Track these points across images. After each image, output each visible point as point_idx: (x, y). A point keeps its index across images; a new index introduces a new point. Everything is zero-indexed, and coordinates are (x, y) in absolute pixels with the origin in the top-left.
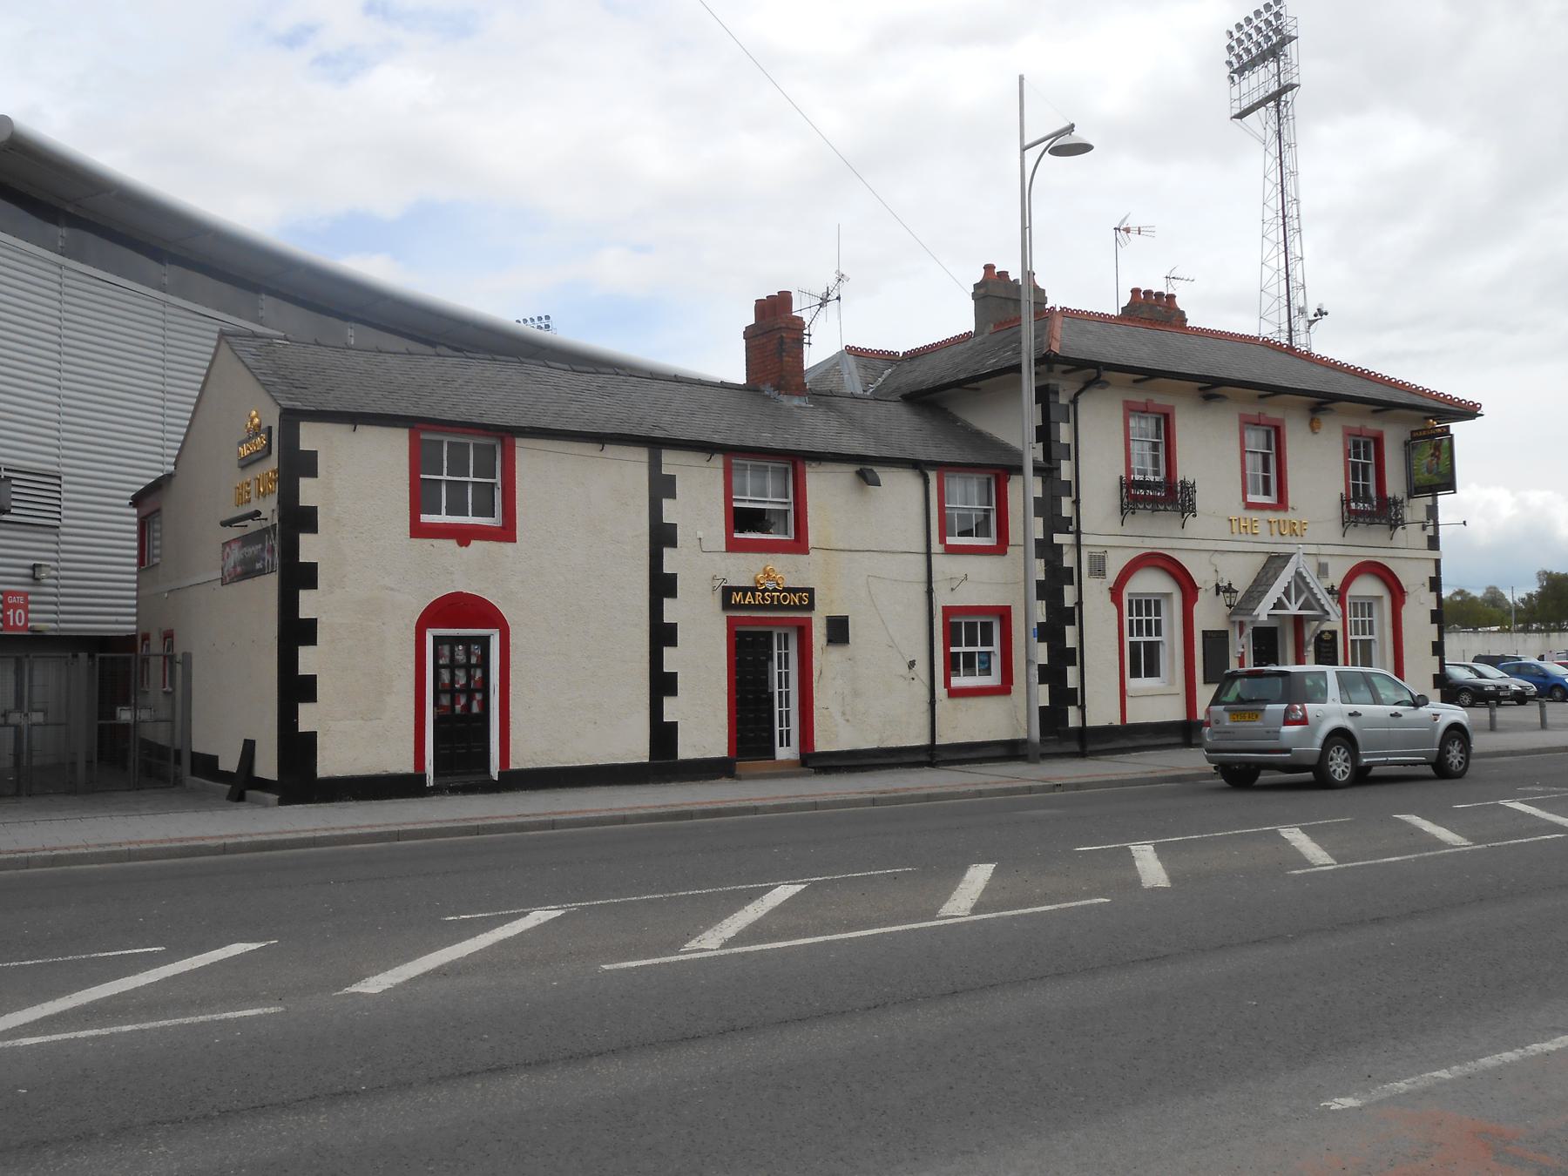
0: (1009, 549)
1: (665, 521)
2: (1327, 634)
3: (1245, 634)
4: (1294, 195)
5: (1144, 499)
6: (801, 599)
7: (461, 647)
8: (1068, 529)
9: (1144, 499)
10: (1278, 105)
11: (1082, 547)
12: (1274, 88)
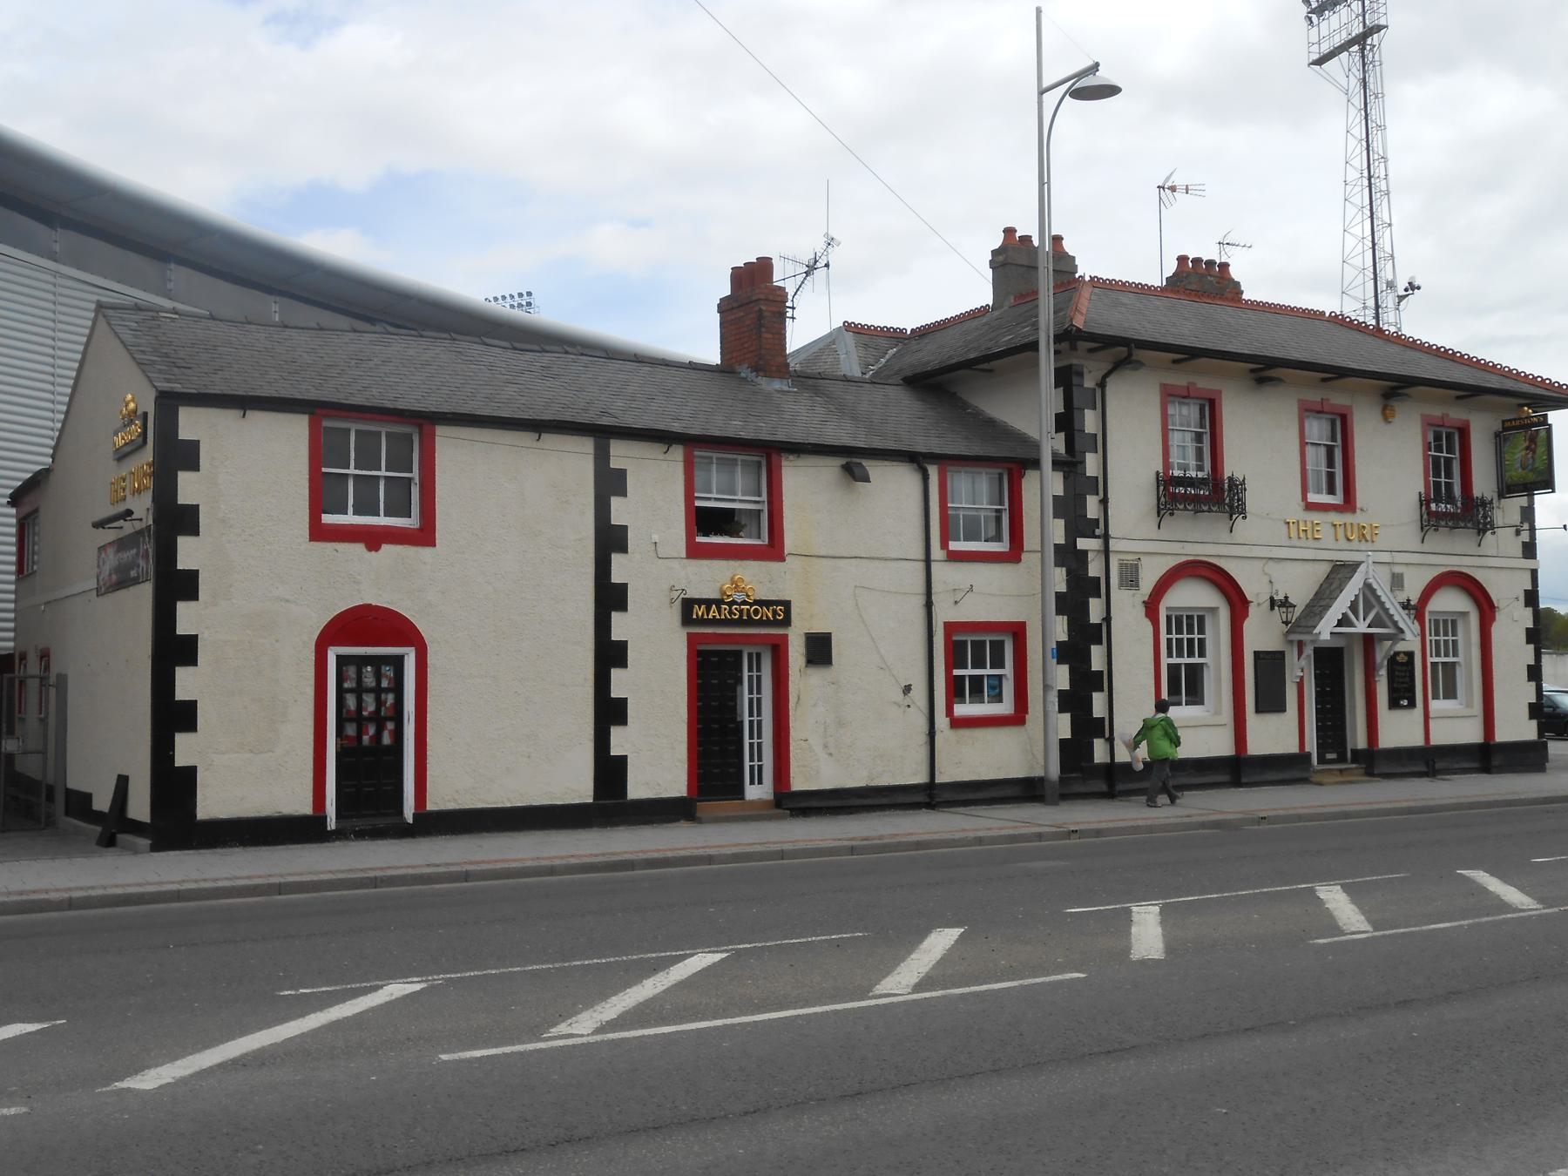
0: (1024, 556)
1: (181, 500)
2: (1402, 655)
3: (1304, 656)
4: (1381, 153)
5: (1185, 498)
6: (775, 613)
7: (369, 669)
8: (1094, 532)
9: (1185, 498)
10: (1363, 50)
11: (1111, 555)
12: (1357, 29)
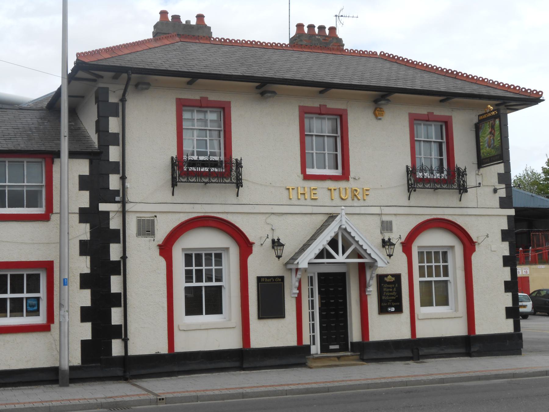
2: (390, 277)
